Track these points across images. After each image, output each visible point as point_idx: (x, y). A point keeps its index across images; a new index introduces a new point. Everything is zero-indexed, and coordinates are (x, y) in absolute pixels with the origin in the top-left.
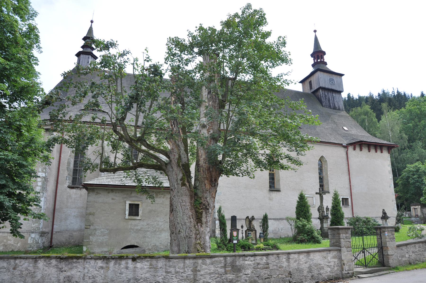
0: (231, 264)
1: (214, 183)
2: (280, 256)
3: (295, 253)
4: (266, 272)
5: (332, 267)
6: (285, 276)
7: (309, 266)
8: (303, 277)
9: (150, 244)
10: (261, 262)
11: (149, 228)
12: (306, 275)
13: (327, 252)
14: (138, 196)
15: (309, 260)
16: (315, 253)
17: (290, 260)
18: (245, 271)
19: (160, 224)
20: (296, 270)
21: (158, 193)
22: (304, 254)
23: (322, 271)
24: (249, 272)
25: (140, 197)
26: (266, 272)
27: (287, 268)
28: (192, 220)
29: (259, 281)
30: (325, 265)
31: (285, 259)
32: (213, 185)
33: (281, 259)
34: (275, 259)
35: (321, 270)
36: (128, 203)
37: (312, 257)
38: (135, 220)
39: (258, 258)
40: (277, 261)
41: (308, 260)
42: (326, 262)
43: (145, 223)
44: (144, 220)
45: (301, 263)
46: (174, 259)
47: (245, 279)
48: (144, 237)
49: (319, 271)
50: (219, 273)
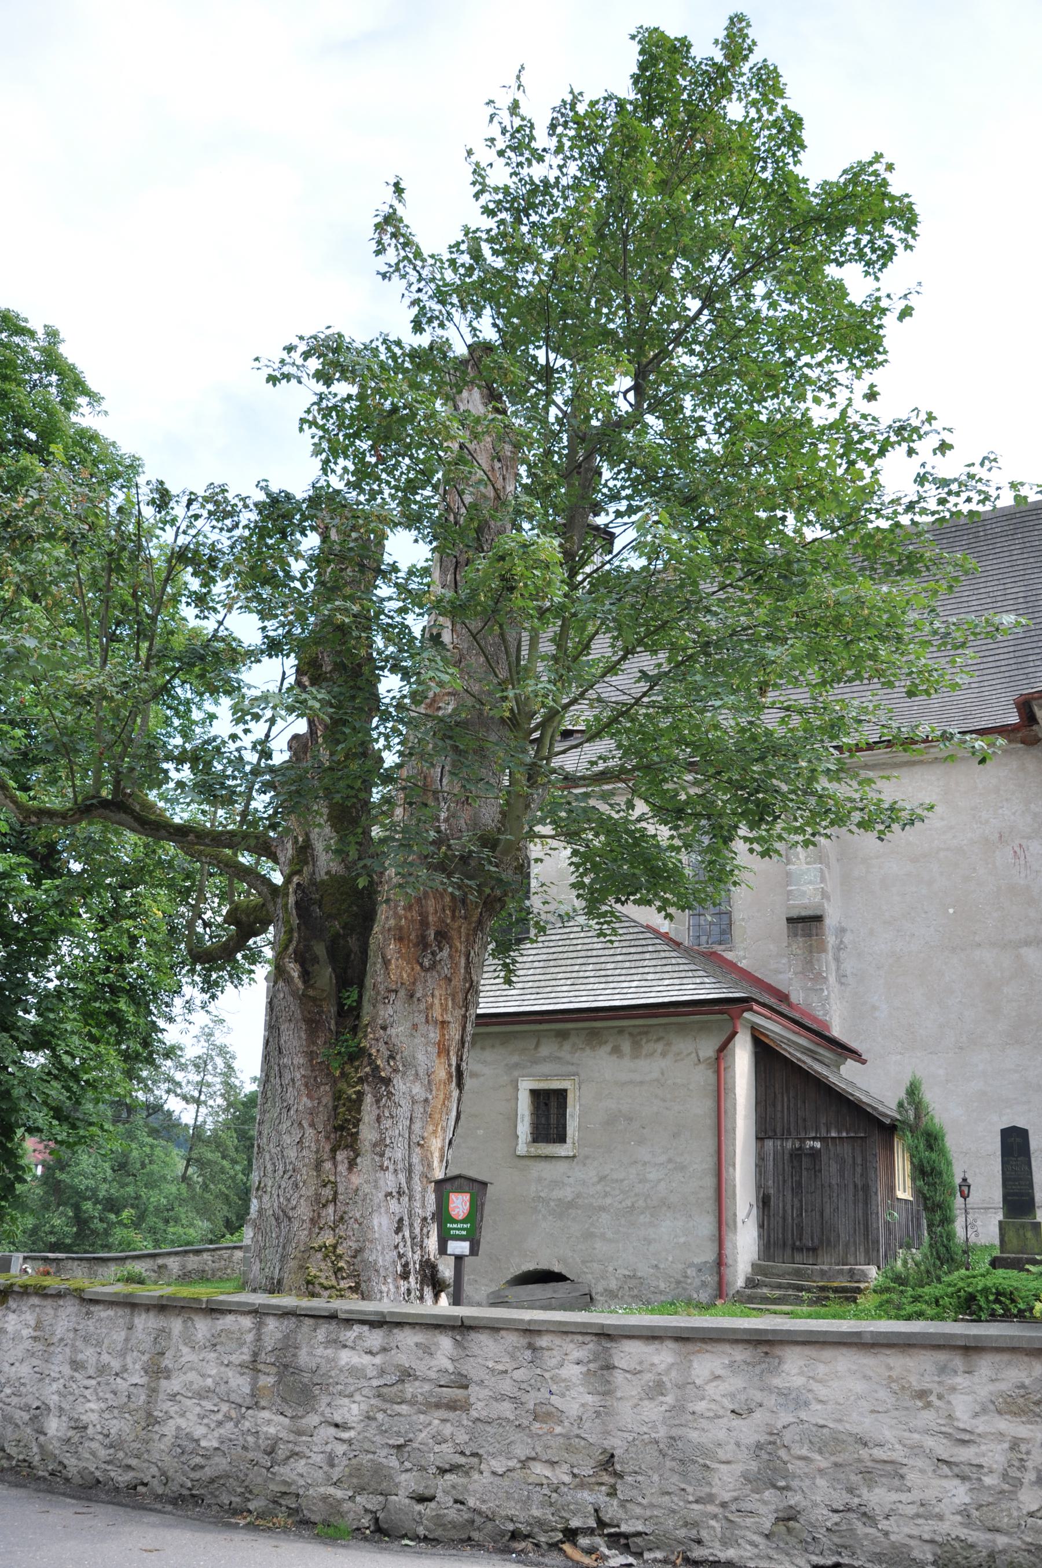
0: (278, 1358)
1: (433, 954)
2: (543, 1341)
3: (652, 1336)
4: (448, 1430)
5: (988, 1480)
6: (567, 1479)
7: (763, 1438)
8: (711, 1508)
9: (611, 1269)
10: (420, 1368)
11: (606, 1195)
12: (727, 1496)
13: (942, 1357)
14: (562, 1054)
15: (771, 1401)
16: (828, 1354)
17: (619, 1377)
18: (329, 1404)
19: (653, 1175)
20: (652, 1450)
21: (640, 1033)
22: (727, 1348)
23: (879, 1497)
24: (351, 1411)
25: (568, 1057)
26: (448, 1430)
27: (587, 1425)
28: (310, 1132)
29: (404, 1477)
30: (916, 1450)
31: (582, 1369)
32: (426, 963)
33: (553, 1362)
34: (513, 1357)
35: (871, 1484)
36: (526, 1086)
37: (799, 1381)
38: (554, 1161)
39: (408, 1338)
40: (518, 1375)
41: (758, 1396)
42: (927, 1432)
43: (590, 1173)
44: (587, 1157)
45: (701, 1406)
46: (100, 1307)
47: (328, 1448)
48: (588, 1236)
49: (851, 1490)
50: (233, 1397)
